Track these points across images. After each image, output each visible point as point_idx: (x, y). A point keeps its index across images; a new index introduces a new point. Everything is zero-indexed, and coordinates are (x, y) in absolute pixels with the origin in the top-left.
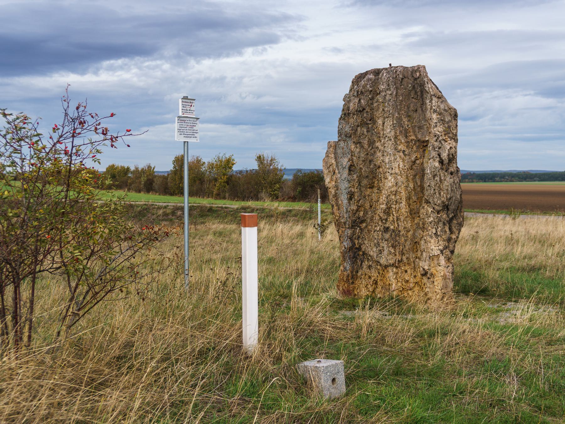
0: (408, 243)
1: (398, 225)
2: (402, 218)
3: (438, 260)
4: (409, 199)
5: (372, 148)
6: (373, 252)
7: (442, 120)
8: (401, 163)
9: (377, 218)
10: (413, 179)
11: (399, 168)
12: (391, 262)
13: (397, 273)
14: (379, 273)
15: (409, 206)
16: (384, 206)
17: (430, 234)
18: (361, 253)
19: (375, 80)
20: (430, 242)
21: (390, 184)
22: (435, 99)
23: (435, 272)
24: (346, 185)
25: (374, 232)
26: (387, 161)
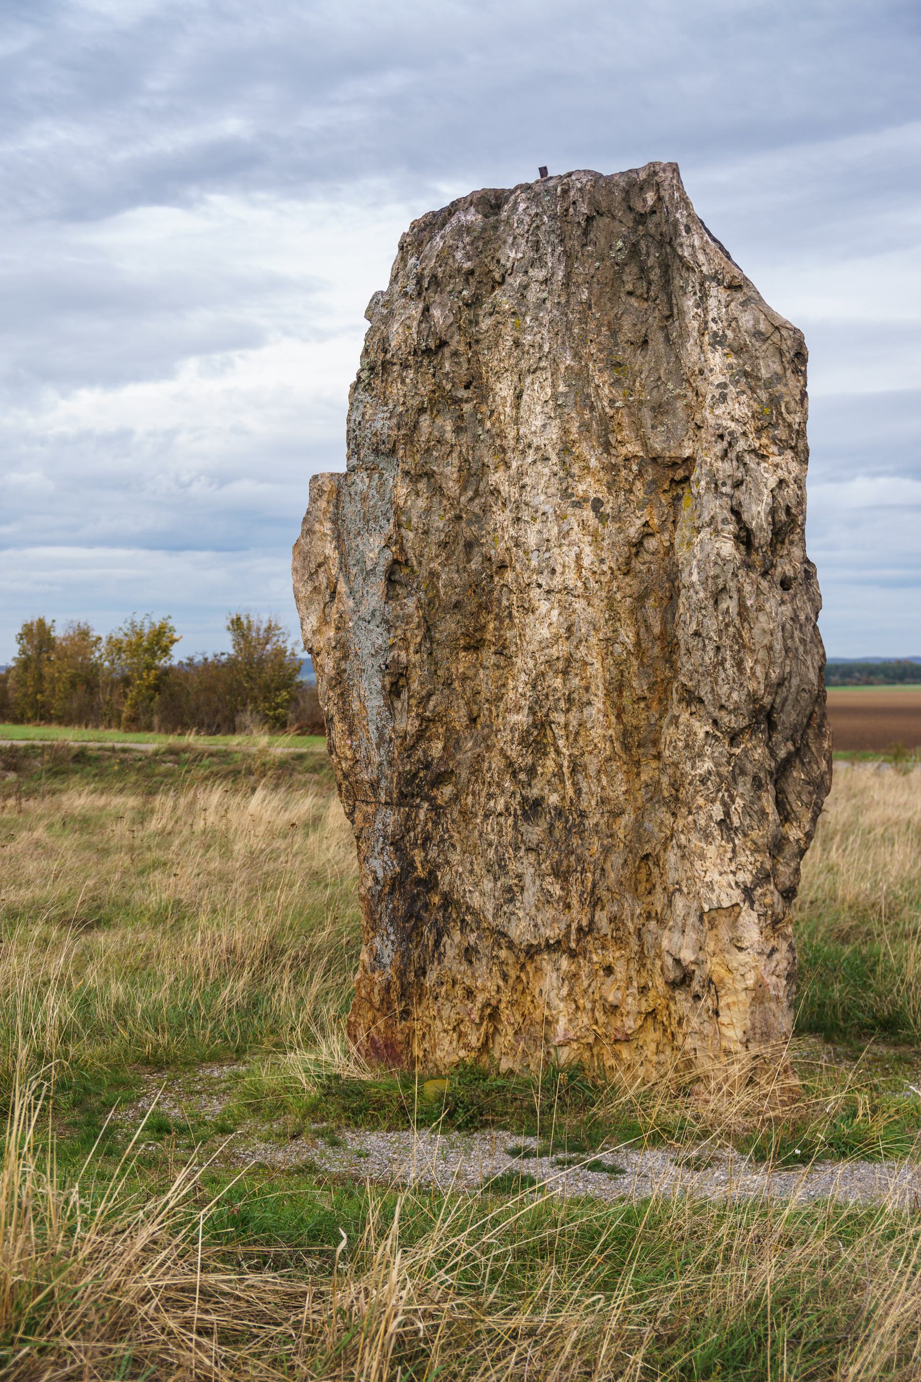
0: (616, 859)
1: (578, 792)
2: (593, 763)
3: (734, 925)
4: (617, 687)
6: (481, 896)
7: (746, 374)
8: (587, 550)
9: (497, 762)
10: (632, 612)
11: (579, 567)
12: (552, 933)
13: (575, 976)
14: (505, 977)
15: (618, 717)
16: (521, 719)
19: (484, 230)
20: (702, 857)
21: (545, 632)
22: (717, 294)
23: (722, 972)
24: (377, 637)
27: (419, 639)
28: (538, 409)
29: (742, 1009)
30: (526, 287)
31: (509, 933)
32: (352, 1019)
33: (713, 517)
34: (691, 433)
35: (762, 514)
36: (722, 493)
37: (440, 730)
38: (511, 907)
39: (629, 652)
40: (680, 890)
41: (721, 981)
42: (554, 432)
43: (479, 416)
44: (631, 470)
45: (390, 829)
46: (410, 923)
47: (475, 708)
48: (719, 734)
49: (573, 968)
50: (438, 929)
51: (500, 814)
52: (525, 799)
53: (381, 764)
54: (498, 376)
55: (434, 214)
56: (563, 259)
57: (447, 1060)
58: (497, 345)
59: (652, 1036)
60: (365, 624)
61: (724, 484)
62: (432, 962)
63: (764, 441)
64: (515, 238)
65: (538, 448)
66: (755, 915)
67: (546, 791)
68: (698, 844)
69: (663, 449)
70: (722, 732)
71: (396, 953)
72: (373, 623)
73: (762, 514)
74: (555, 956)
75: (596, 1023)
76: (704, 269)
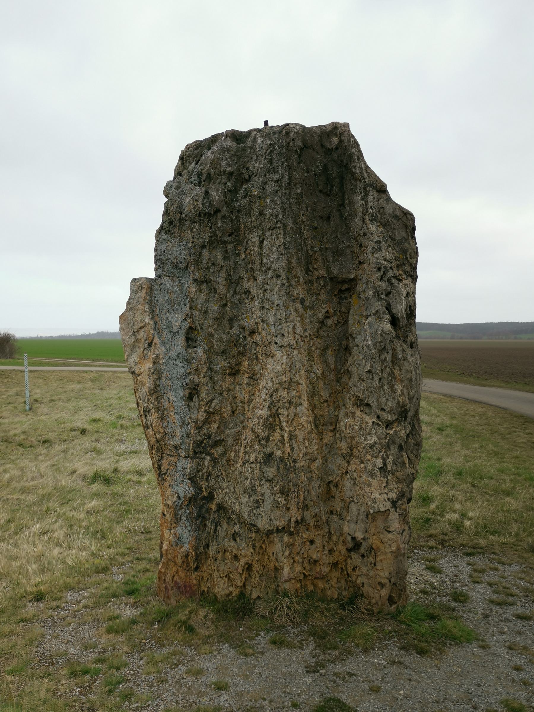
0: (316, 484)
1: (292, 449)
2: (301, 435)
3: (386, 519)
4: (313, 394)
5: (235, 292)
6: (242, 505)
8: (298, 324)
9: (250, 435)
10: (320, 356)
11: (295, 333)
12: (280, 523)
13: (292, 545)
16: (263, 412)
17: (370, 468)
18: (213, 507)
19: (238, 150)
20: (369, 485)
23: (379, 543)
24: (181, 369)
25: (244, 464)
26: (271, 319)
27: (205, 370)
28: (275, 249)
29: (389, 562)
30: (265, 183)
31: (257, 525)
32: (163, 570)
33: (377, 311)
34: (355, 265)
35: (403, 310)
36: (381, 298)
37: (217, 418)
38: (258, 511)
39: (318, 377)
40: (353, 501)
41: (378, 548)
42: (283, 262)
43: (237, 252)
44: (320, 284)
45: (188, 471)
46: (200, 520)
47: (235, 405)
48: (380, 423)
49: (291, 540)
50: (216, 523)
51: (252, 463)
52: (265, 454)
53: (182, 436)
54: (250, 230)
55: (200, 142)
56: (287, 170)
57: (223, 593)
58: (250, 214)
59: (336, 574)
60: (174, 361)
61: (382, 294)
62: (213, 541)
63: (401, 272)
64: (257, 156)
65: (275, 270)
66: (397, 514)
67: (275, 449)
68: (367, 479)
69: (339, 274)
70: (382, 422)
71: (192, 537)
72: (178, 360)
73: (403, 310)
74: (280, 535)
75: (305, 568)
76: (367, 180)
